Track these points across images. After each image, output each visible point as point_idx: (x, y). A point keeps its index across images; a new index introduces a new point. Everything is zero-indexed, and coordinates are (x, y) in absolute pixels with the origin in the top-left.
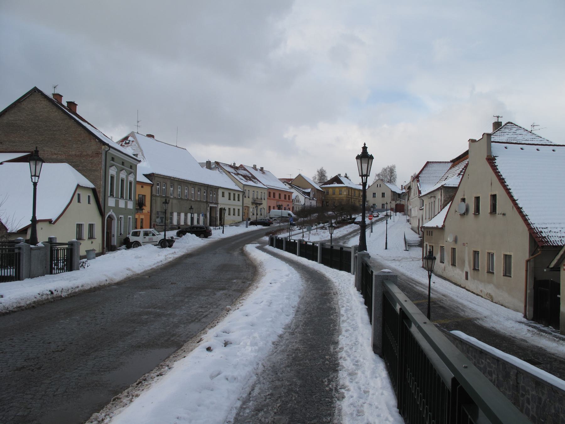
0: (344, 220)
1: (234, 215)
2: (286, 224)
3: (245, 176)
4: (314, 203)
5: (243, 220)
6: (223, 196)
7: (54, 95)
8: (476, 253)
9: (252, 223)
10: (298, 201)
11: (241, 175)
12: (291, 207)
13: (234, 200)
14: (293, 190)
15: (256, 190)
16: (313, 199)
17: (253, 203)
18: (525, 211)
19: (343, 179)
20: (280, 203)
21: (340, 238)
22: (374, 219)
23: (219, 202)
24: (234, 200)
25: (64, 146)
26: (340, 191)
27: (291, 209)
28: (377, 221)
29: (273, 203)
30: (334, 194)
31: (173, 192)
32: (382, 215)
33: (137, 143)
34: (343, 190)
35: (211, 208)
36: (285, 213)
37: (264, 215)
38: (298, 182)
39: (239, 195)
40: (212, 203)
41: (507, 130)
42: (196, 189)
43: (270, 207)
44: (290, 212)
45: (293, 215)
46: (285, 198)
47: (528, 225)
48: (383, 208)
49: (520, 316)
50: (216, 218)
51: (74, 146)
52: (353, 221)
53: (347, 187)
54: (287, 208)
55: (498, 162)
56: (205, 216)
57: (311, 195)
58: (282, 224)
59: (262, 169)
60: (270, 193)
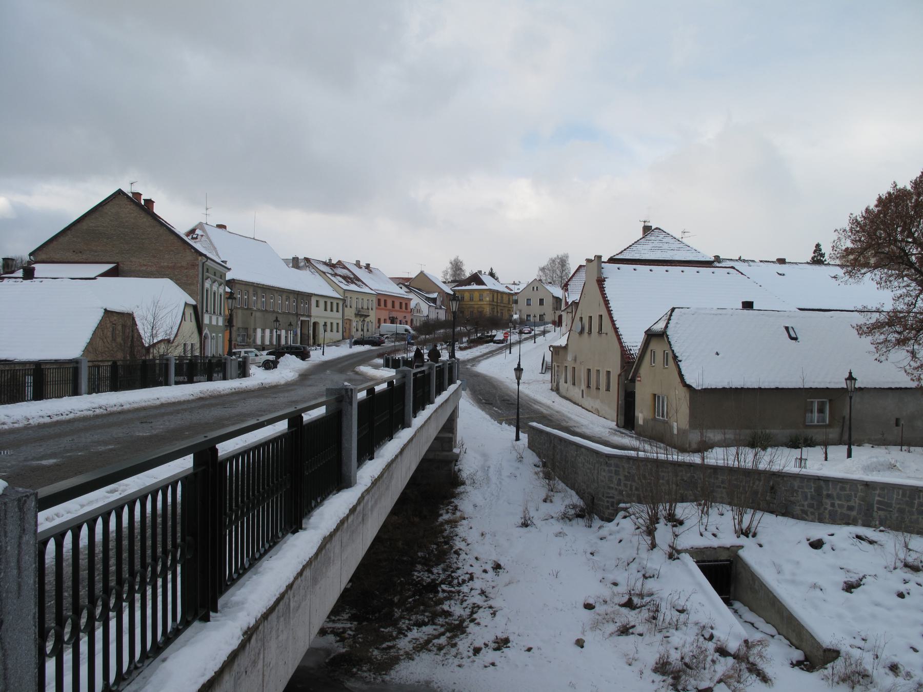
0: (480, 338)
1: (331, 331)
2: (403, 343)
3: (344, 278)
4: (442, 315)
5: (344, 338)
6: (317, 306)
7: (133, 194)
8: (589, 370)
9: (357, 343)
10: (419, 311)
11: (340, 276)
12: (409, 319)
13: (332, 310)
14: (411, 296)
15: (360, 297)
16: (441, 308)
17: (357, 315)
18: (621, 331)
19: (486, 278)
20: (394, 314)
21: (469, 361)
22: (524, 336)
23: (313, 314)
24: (332, 310)
25: (155, 257)
26: (481, 295)
27: (409, 322)
28: (526, 339)
29: (384, 315)
30: (471, 299)
31: (257, 302)
32: (538, 330)
33: (208, 238)
34: (485, 294)
35: (302, 321)
36: (401, 328)
37: (372, 331)
38: (419, 284)
39: (338, 304)
40: (303, 315)
41: (653, 238)
42: (284, 297)
43: (379, 320)
44: (408, 327)
45: (412, 332)
46: (401, 308)
47: (621, 343)
48: (542, 320)
49: (613, 425)
50: (308, 336)
51: (167, 257)
52: (491, 339)
53: (490, 290)
54: (404, 321)
55: (607, 284)
56: (295, 334)
57: (438, 303)
58: (397, 343)
59: (368, 266)
60: (379, 300)
